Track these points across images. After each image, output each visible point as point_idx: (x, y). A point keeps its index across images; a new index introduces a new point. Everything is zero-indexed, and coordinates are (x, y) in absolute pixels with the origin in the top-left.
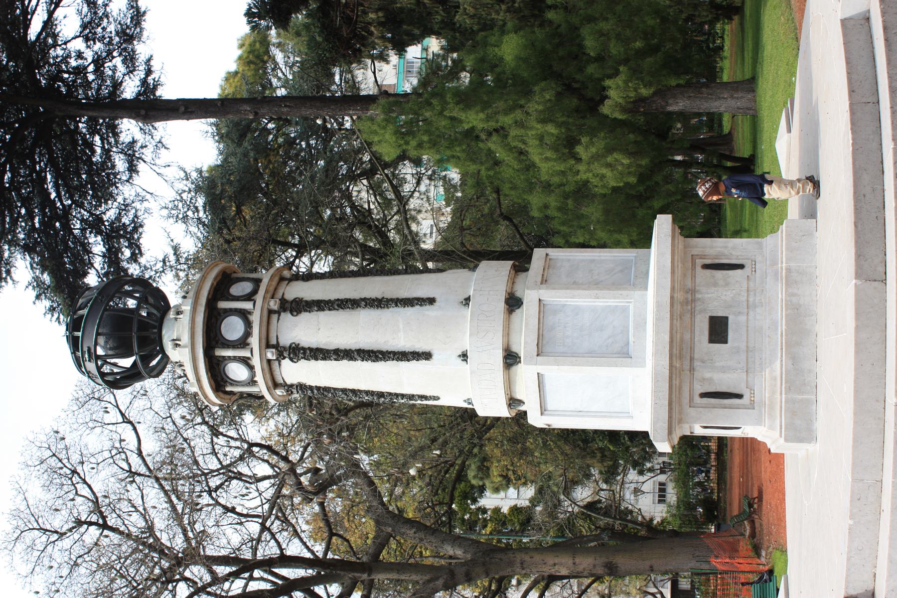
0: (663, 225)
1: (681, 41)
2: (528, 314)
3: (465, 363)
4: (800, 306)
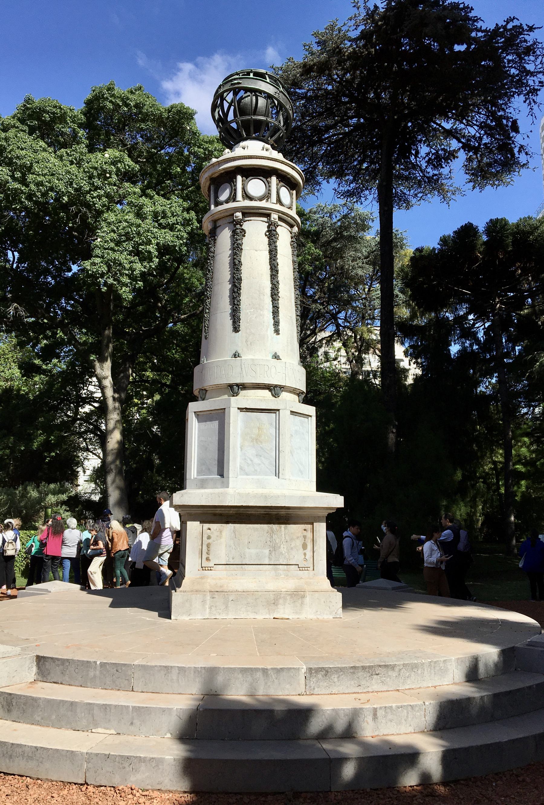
0: (336, 501)
1: (44, 367)
3: (445, 204)
4: (276, 605)
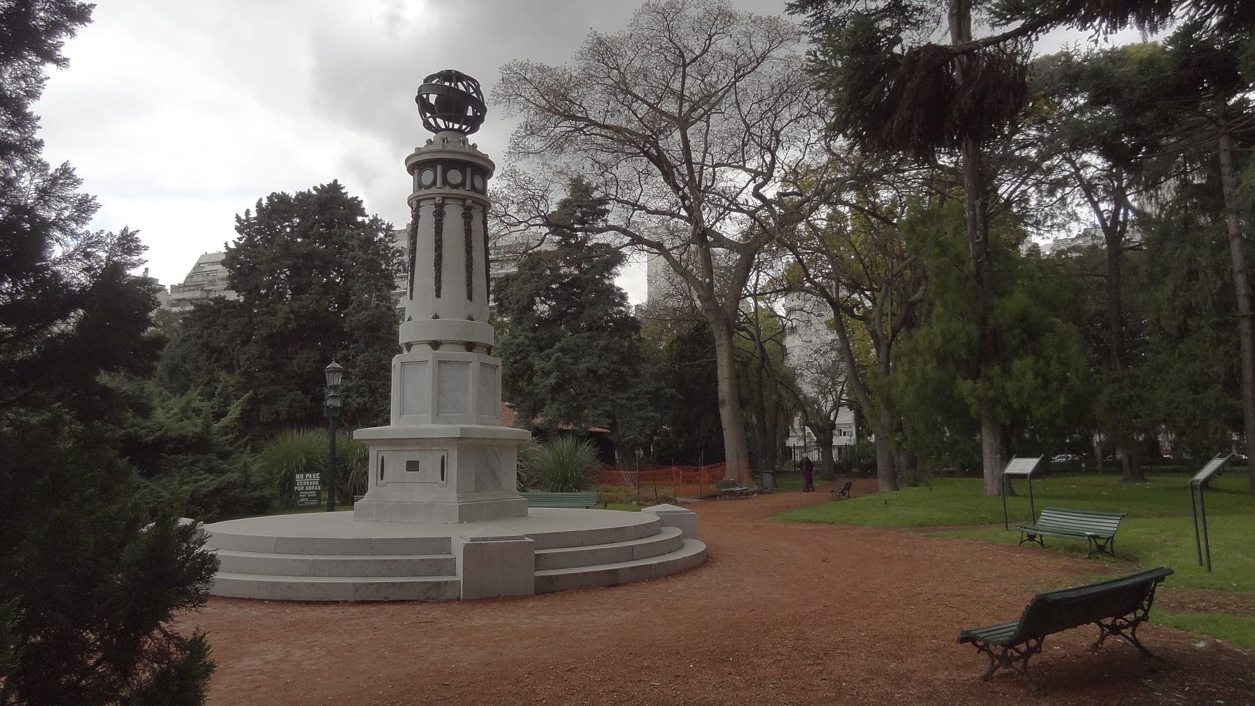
2: (464, 355)
